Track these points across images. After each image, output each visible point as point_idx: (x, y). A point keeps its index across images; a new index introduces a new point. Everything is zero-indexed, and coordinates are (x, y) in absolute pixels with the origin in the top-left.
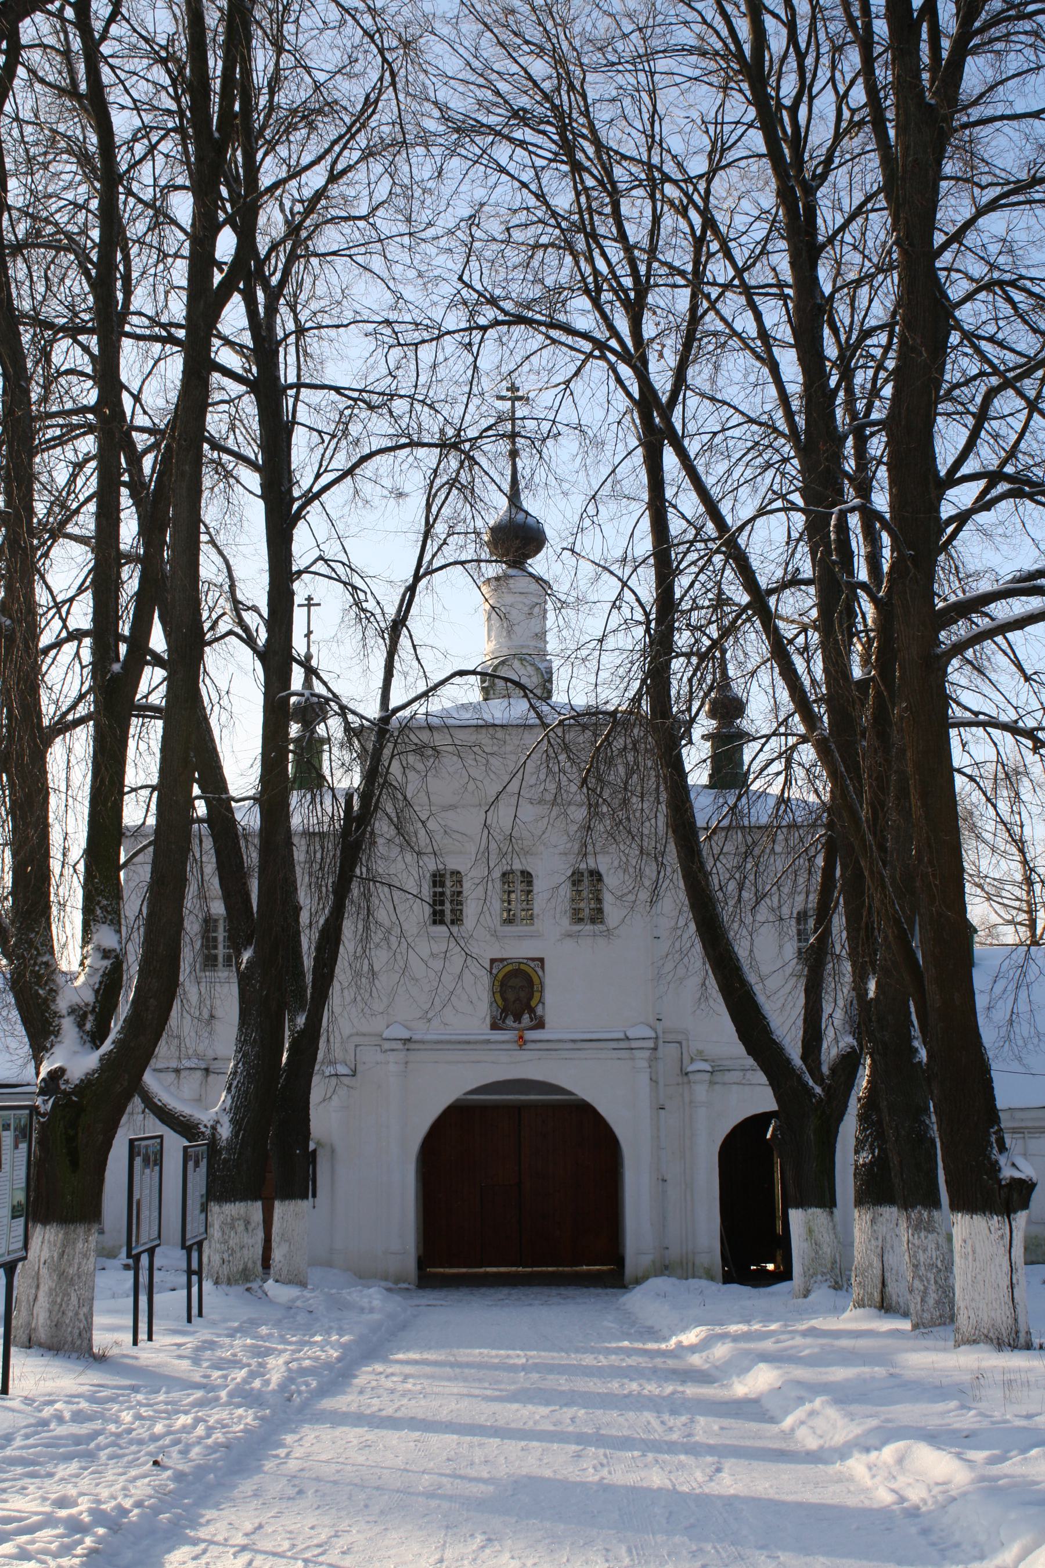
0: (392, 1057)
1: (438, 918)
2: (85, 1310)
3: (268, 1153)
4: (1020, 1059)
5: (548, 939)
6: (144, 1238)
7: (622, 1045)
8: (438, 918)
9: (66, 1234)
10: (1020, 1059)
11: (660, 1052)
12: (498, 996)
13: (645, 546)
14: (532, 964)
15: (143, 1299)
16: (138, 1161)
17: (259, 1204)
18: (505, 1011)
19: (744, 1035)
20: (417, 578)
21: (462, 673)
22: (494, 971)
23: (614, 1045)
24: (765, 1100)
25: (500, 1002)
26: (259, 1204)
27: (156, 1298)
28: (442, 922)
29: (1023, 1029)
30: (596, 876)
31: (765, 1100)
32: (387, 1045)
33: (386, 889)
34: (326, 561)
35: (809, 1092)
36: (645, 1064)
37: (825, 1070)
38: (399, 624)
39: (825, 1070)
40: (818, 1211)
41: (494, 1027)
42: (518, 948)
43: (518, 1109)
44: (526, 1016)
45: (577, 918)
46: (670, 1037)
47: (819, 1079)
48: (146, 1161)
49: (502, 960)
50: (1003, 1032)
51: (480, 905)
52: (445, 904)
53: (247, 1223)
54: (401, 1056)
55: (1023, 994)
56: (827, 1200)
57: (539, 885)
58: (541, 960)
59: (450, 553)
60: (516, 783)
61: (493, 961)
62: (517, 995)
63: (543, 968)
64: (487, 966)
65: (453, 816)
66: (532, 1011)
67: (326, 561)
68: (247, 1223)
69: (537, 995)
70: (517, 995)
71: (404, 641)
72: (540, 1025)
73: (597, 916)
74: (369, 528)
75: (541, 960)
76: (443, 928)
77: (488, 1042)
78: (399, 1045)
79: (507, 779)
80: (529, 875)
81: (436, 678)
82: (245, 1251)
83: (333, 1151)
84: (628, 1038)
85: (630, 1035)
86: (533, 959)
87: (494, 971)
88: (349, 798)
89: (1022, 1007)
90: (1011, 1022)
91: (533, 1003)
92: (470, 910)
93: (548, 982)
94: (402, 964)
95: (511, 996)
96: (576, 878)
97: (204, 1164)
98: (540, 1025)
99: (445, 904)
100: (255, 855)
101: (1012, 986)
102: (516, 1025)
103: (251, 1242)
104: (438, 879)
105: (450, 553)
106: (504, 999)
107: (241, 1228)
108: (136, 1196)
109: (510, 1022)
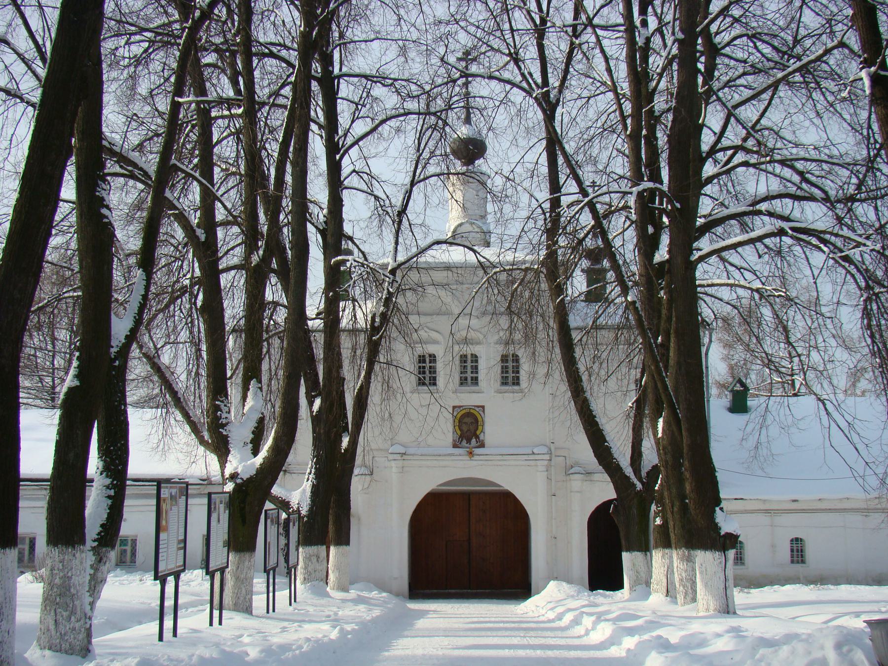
0: (393, 464)
1: (421, 383)
2: (249, 596)
3: (328, 519)
4: (763, 469)
5: (488, 395)
6: (271, 563)
7: (532, 457)
8: (421, 383)
9: (240, 558)
10: (763, 469)
11: (553, 463)
12: (457, 428)
13: (511, 395)
14: (477, 409)
15: (271, 594)
16: (269, 521)
17: (324, 547)
18: (461, 437)
19: (598, 455)
20: (413, 184)
21: (438, 243)
22: (455, 414)
23: (526, 457)
24: (610, 493)
25: (459, 432)
26: (324, 547)
27: (277, 593)
28: (424, 384)
29: (763, 451)
30: (516, 359)
31: (610, 493)
32: (391, 457)
33: (394, 368)
34: (357, 173)
35: (634, 485)
36: (544, 469)
37: (644, 474)
38: (402, 212)
39: (644, 474)
40: (639, 553)
41: (455, 446)
42: (469, 399)
43: (467, 496)
44: (474, 440)
45: (504, 383)
46: (559, 453)
47: (640, 479)
48: (272, 521)
49: (460, 407)
50: (752, 453)
51: (447, 373)
52: (426, 372)
53: (318, 557)
54: (400, 463)
55: (764, 431)
56: (645, 548)
57: (482, 365)
58: (483, 407)
59: (432, 169)
60: (469, 307)
61: (454, 407)
62: (469, 428)
63: (484, 411)
64: (451, 410)
65: (435, 329)
66: (477, 437)
67: (357, 173)
68: (318, 557)
69: (480, 428)
70: (469, 428)
71: (405, 220)
72: (482, 445)
73: (516, 382)
74: (386, 159)
75: (483, 407)
76: (426, 388)
77: (452, 455)
78: (398, 457)
79: (464, 304)
80: (476, 357)
81: (423, 244)
82: (317, 573)
83: (359, 520)
84: (533, 453)
85: (535, 451)
86: (478, 407)
87: (455, 414)
88: (373, 318)
89: (763, 438)
90: (756, 448)
91: (478, 433)
92: (441, 381)
93: (487, 420)
94: (403, 411)
95: (465, 428)
96: (504, 359)
97: (297, 524)
98: (482, 445)
99: (426, 372)
100: (321, 352)
101: (758, 427)
102: (468, 445)
103: (320, 568)
104: (422, 359)
105: (432, 169)
106: (461, 430)
107: (314, 559)
108: (268, 541)
109: (464, 443)
